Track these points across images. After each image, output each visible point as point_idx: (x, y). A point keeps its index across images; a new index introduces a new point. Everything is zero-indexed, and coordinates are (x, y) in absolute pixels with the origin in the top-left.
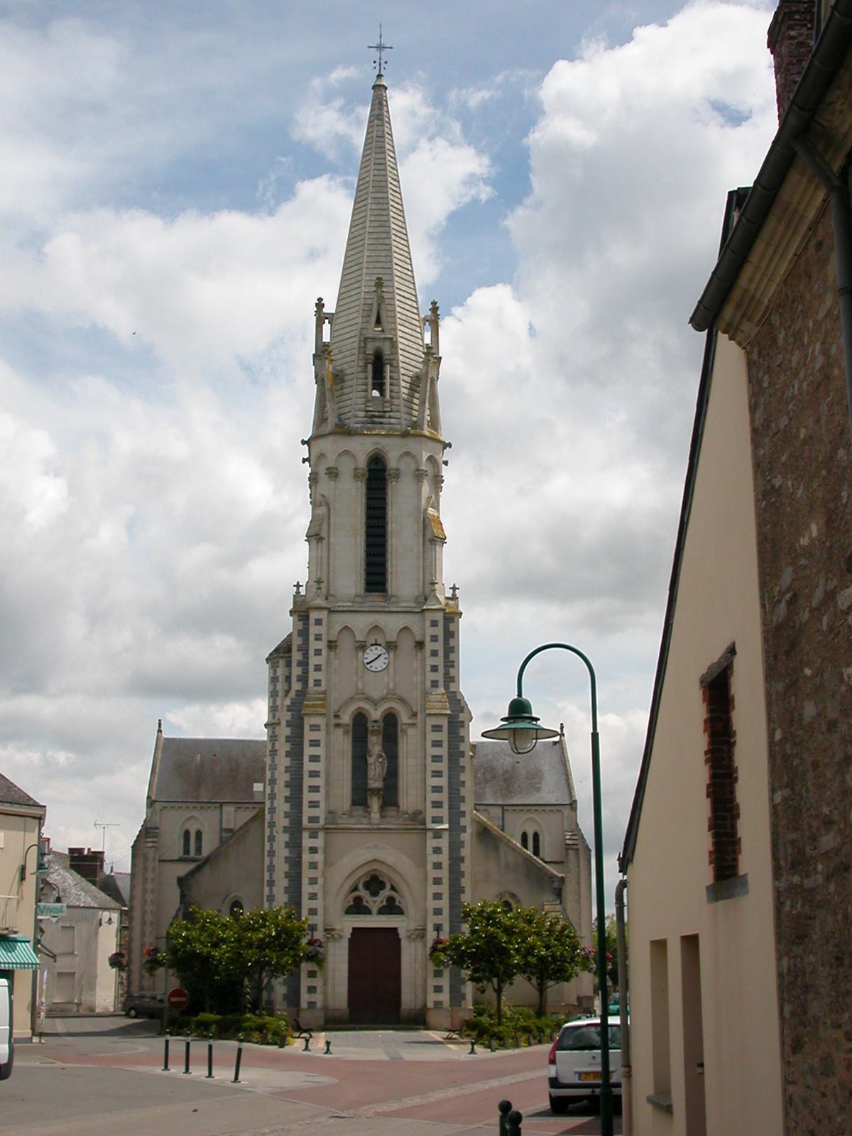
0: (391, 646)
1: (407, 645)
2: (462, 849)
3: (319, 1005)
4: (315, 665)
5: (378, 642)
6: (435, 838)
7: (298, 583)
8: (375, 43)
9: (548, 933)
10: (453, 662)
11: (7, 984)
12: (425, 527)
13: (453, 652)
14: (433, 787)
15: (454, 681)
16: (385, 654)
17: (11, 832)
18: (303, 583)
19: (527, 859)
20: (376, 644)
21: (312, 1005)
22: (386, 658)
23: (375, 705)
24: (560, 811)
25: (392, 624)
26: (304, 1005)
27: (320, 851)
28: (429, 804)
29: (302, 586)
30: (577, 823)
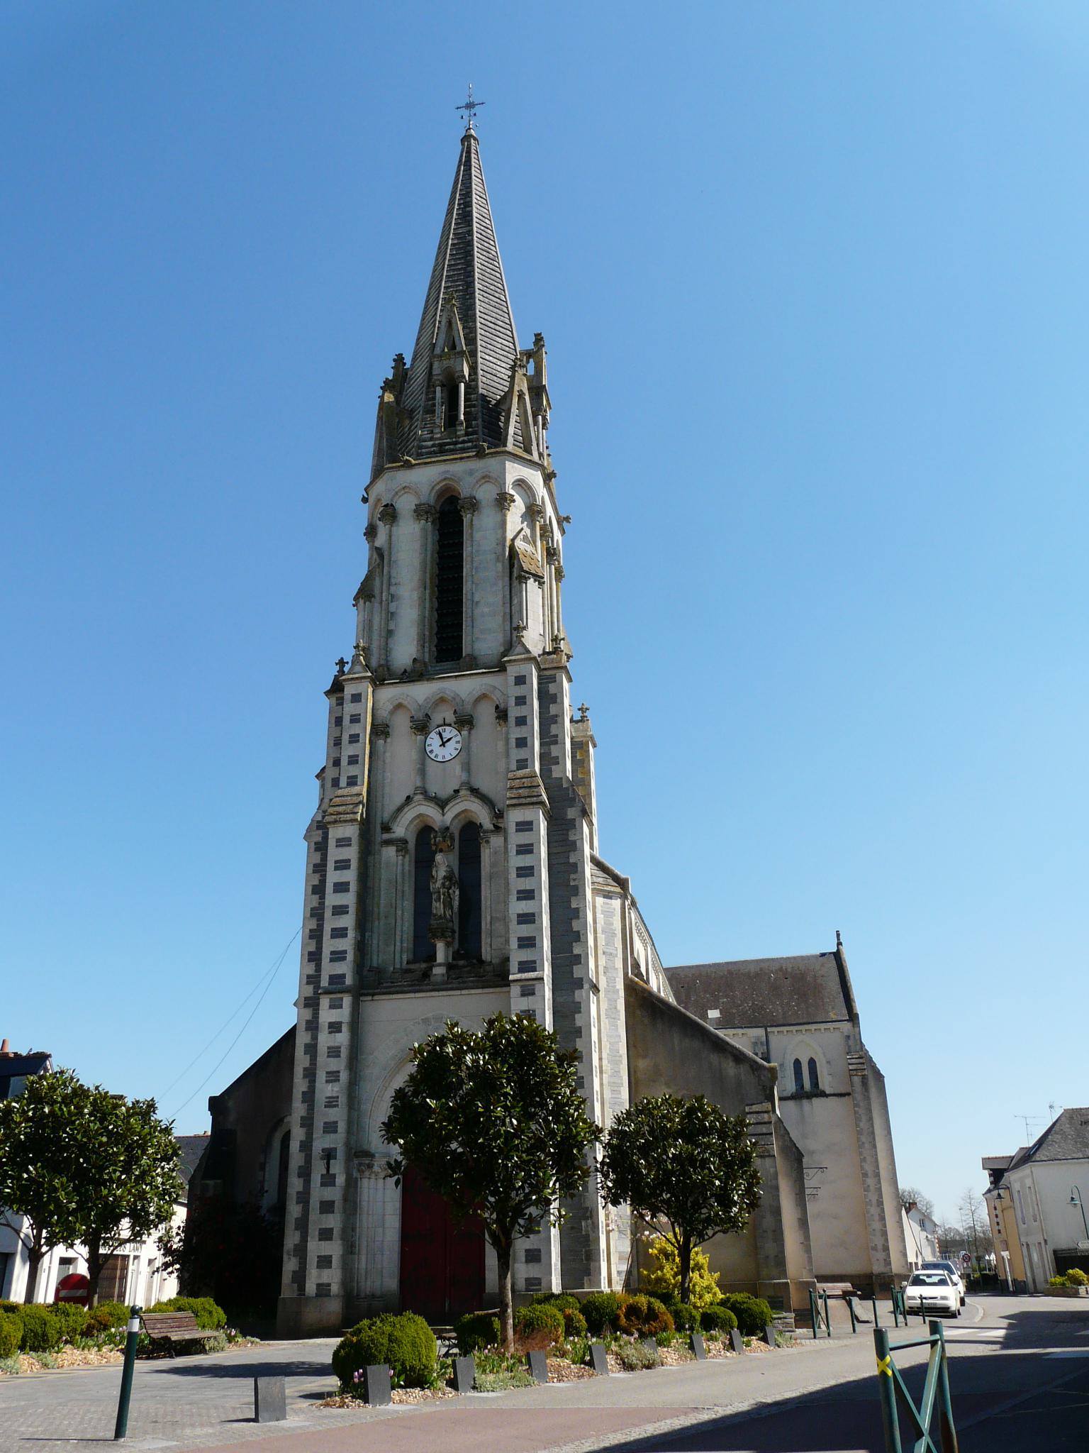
0: (465, 722)
1: (485, 715)
2: (577, 1016)
3: (335, 1288)
4: (349, 757)
5: (447, 722)
6: (523, 995)
7: (444, 746)
8: (476, 110)
9: (515, 1019)
10: (556, 736)
11: (47, 1302)
12: (512, 566)
13: (556, 722)
14: (519, 915)
15: (558, 763)
16: (456, 736)
17: (798, 1394)
18: (348, 658)
19: (644, 998)
20: (445, 725)
21: (323, 1290)
22: (457, 742)
23: (443, 808)
24: (839, 1028)
25: (464, 687)
26: (311, 1288)
27: (345, 1028)
28: (514, 944)
29: (347, 663)
30: (861, 1042)
